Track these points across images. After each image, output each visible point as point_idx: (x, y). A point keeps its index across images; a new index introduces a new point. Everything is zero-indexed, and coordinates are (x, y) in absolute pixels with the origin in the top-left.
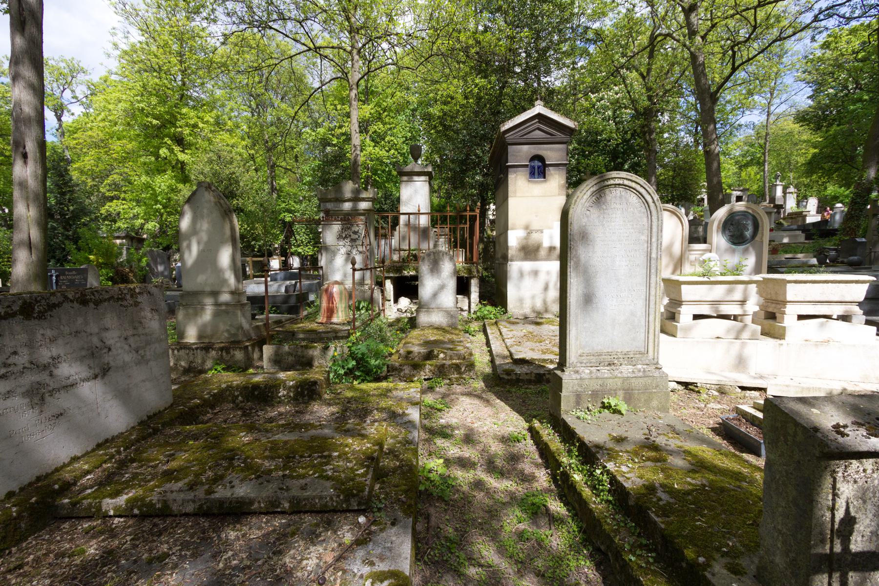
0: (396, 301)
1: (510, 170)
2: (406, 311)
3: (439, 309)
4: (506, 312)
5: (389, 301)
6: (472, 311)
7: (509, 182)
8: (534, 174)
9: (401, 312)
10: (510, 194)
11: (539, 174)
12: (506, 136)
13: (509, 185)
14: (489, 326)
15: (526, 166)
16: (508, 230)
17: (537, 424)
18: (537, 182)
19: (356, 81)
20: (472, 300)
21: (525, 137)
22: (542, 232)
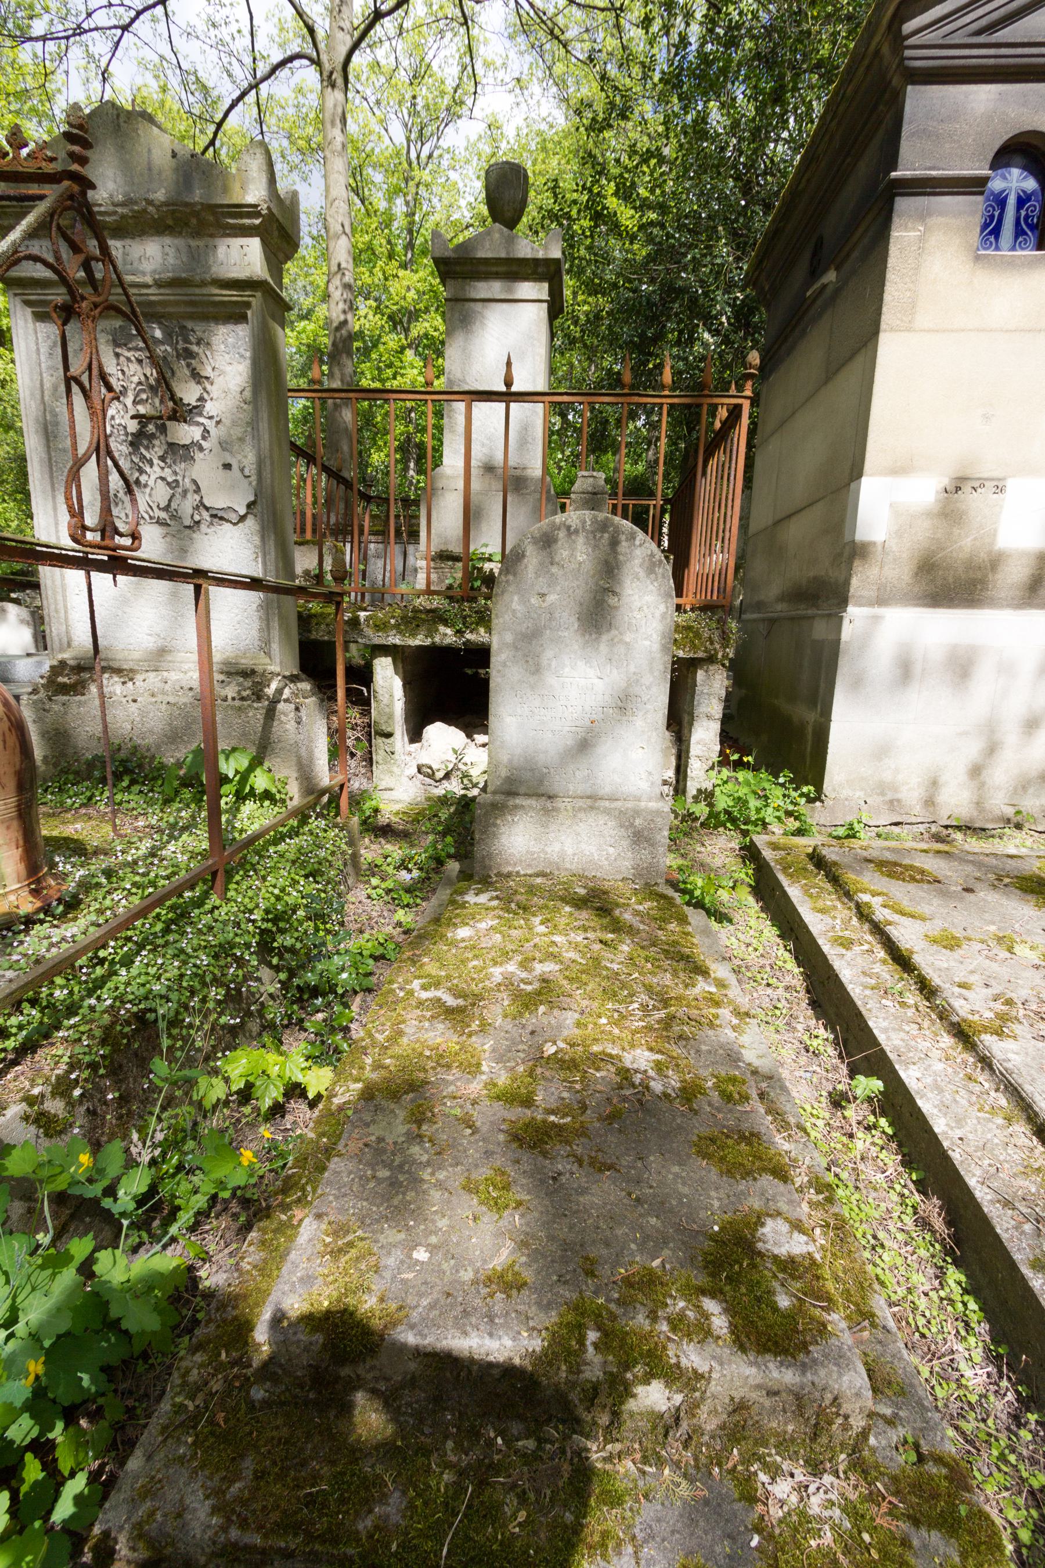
0: (415, 735)
1: (903, 204)
2: (447, 776)
3: (593, 801)
4: (818, 797)
5: (389, 735)
6: (692, 789)
7: (892, 261)
8: (996, 232)
9: (432, 776)
10: (888, 317)
11: (1019, 232)
12: (909, 27)
13: (890, 276)
14: (184, 559)
15: (974, 185)
16: (856, 472)
17: (114, 218)
18: (1011, 264)
19: (341, 58)
20: (695, 749)
21: (1003, 35)
22: (1000, 489)
